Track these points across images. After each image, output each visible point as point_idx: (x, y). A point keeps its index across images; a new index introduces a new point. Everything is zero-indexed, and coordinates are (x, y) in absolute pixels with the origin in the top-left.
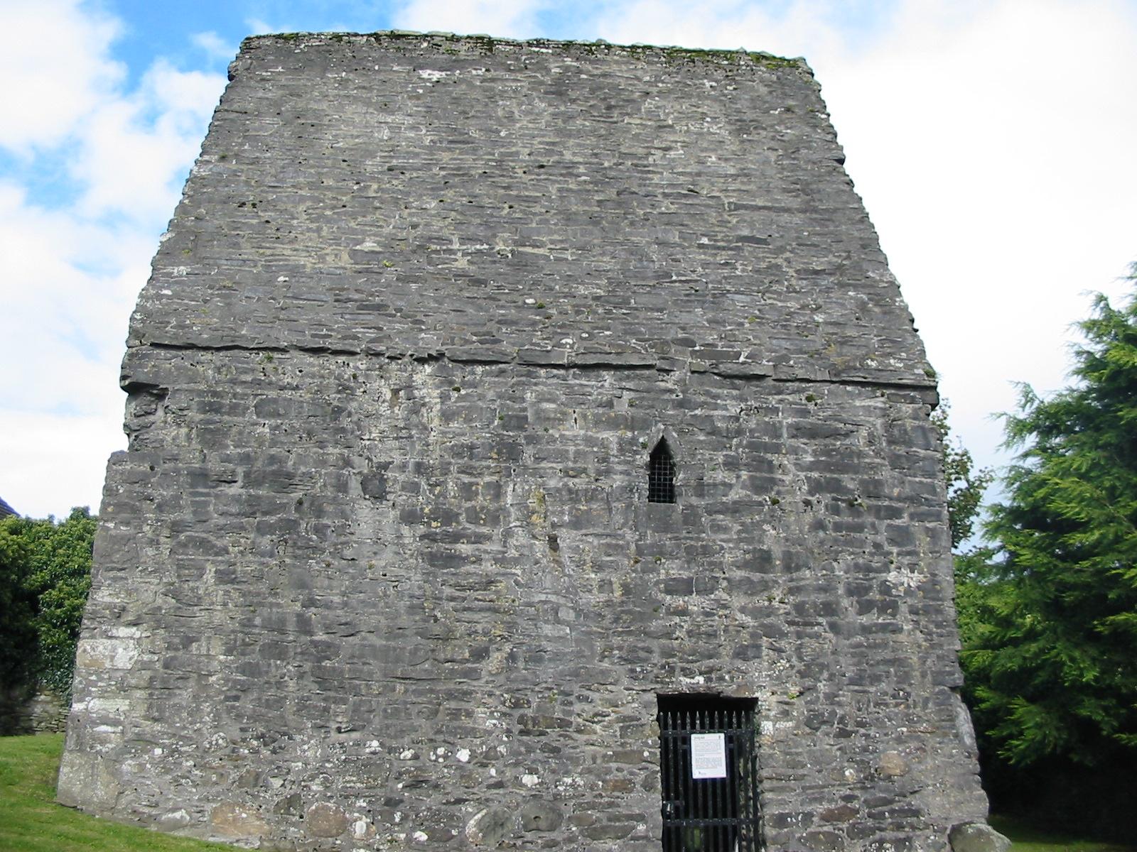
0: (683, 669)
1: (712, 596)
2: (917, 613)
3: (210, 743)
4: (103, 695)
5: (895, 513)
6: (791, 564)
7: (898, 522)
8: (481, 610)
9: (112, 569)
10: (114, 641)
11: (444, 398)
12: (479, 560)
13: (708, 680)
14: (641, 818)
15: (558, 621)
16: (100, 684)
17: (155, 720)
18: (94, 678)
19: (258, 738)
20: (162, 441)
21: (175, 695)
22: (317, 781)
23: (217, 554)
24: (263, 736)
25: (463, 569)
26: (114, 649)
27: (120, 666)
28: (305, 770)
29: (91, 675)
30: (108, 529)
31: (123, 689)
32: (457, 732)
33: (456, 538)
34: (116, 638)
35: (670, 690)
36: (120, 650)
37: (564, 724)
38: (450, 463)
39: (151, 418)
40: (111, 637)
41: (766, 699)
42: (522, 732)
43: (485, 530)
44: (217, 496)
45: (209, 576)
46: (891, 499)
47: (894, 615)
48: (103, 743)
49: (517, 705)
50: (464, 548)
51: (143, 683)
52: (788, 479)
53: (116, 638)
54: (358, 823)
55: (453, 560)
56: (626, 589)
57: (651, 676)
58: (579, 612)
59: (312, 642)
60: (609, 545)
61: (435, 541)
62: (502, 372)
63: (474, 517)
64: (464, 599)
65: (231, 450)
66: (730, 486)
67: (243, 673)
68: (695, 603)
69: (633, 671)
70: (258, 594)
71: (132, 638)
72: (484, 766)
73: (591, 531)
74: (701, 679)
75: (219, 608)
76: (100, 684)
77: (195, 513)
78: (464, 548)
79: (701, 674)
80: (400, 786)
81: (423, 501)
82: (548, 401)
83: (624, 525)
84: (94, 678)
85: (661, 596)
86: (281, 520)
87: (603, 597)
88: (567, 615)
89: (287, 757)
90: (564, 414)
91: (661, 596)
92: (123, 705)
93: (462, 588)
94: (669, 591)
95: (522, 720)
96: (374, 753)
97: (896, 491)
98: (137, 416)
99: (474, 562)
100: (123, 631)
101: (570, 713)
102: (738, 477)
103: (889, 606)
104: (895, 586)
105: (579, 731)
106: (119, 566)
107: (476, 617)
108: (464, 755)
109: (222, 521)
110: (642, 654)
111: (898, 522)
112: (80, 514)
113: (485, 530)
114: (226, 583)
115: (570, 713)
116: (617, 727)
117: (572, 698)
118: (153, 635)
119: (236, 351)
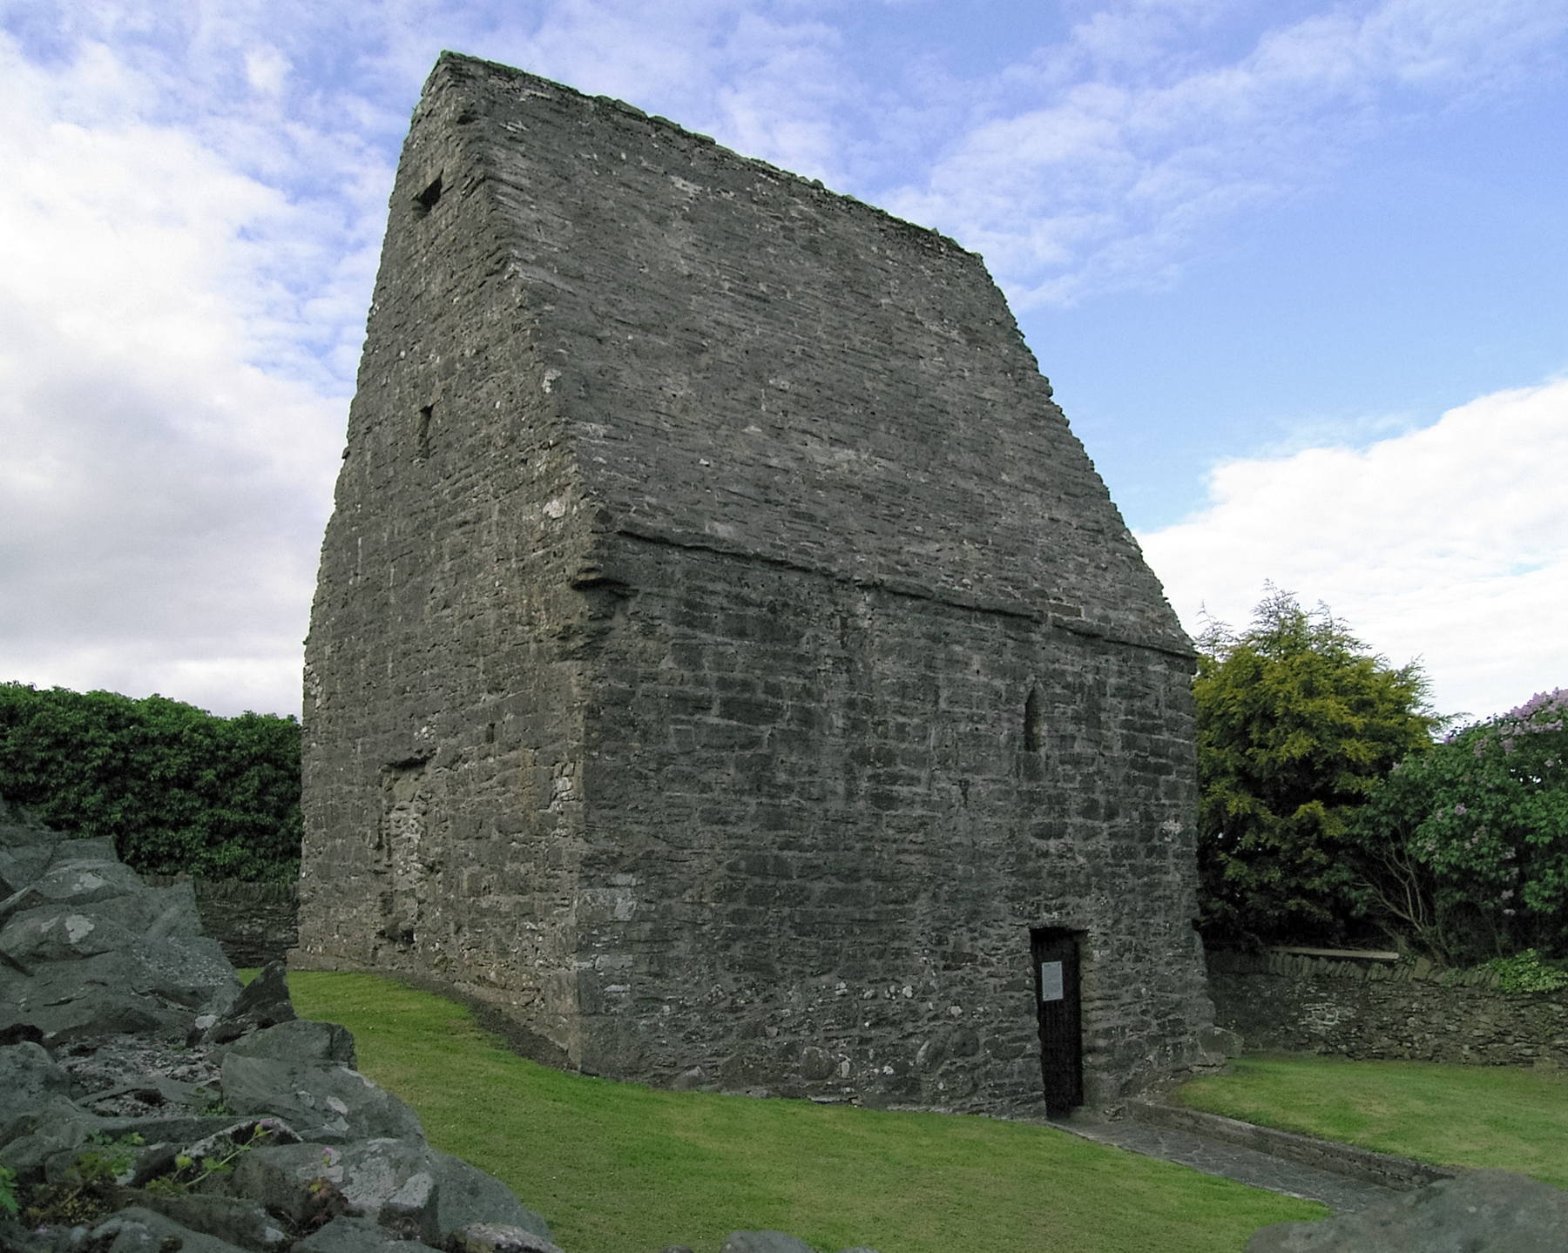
3: (711, 995)
4: (608, 949)
6: (1111, 814)
8: (916, 852)
14: (1028, 1038)
16: (603, 939)
17: (656, 975)
18: (595, 932)
19: (750, 988)
21: (673, 947)
22: (806, 1026)
24: (753, 985)
26: (613, 900)
27: (621, 917)
28: (794, 1015)
29: (593, 929)
31: (627, 944)
32: (893, 975)
33: (894, 779)
34: (614, 886)
35: (1037, 925)
36: (619, 900)
37: (973, 959)
39: (608, 623)
40: (609, 886)
41: (1094, 931)
42: (946, 968)
46: (1167, 757)
48: (616, 1002)
49: (940, 943)
50: (903, 790)
51: (643, 937)
53: (614, 886)
54: (843, 1063)
57: (1026, 913)
62: (924, 608)
67: (733, 921)
68: (1052, 845)
70: (742, 837)
71: (630, 886)
72: (923, 1000)
74: (1055, 914)
75: (707, 851)
76: (603, 939)
77: (679, 744)
78: (903, 790)
80: (867, 1024)
84: (595, 932)
89: (777, 1004)
92: (627, 959)
95: (944, 956)
96: (844, 995)
98: (591, 619)
100: (621, 879)
105: (983, 965)
106: (611, 803)
107: (912, 859)
108: (907, 991)
109: (705, 755)
112: (292, 718)
116: (1006, 960)
118: (648, 882)
119: (705, 553)
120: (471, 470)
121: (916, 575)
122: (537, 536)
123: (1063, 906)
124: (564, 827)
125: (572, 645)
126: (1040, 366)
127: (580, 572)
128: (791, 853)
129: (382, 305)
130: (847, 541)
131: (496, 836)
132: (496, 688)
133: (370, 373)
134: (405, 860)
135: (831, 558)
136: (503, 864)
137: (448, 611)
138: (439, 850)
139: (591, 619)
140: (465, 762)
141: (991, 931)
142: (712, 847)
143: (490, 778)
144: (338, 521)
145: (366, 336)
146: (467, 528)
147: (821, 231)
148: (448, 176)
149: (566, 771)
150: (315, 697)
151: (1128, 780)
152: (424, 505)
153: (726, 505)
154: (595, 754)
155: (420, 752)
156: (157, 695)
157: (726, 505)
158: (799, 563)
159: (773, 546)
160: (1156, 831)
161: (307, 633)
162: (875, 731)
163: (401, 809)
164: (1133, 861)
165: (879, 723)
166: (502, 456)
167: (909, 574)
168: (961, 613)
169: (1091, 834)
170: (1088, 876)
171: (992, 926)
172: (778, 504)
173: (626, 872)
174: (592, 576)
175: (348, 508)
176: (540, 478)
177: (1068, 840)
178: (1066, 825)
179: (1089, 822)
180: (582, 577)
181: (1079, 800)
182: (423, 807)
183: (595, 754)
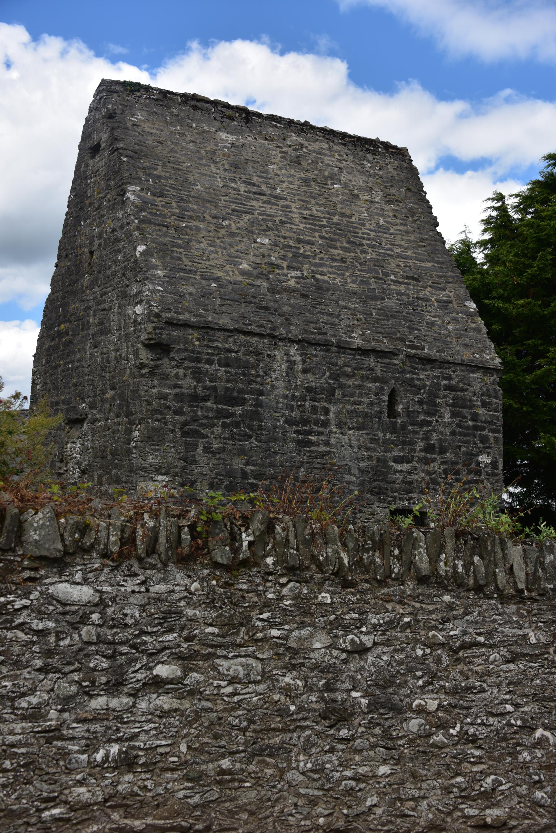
0: (400, 498)
1: (427, 467)
2: (489, 475)
5: (484, 429)
6: (443, 451)
7: (484, 433)
9: (153, 445)
10: (155, 483)
11: (304, 361)
12: (319, 445)
13: (409, 503)
15: (351, 474)
20: (168, 375)
23: (203, 438)
25: (312, 448)
30: (149, 423)
33: (309, 433)
38: (306, 396)
39: (161, 362)
40: (154, 481)
43: (321, 429)
44: (202, 408)
45: (200, 450)
47: (480, 476)
52: (442, 410)
55: (309, 443)
56: (378, 460)
58: (360, 470)
59: (248, 483)
60: (372, 439)
61: (300, 434)
63: (317, 422)
64: (313, 463)
65: (208, 384)
66: (419, 413)
68: (404, 467)
69: (380, 498)
73: (364, 432)
79: (407, 500)
81: (296, 414)
82: (348, 366)
83: (378, 429)
85: (392, 464)
86: (232, 421)
87: (369, 463)
88: (355, 471)
90: (354, 373)
91: (392, 464)
93: (312, 458)
94: (395, 461)
97: (484, 419)
99: (317, 445)
101: (356, 518)
102: (423, 408)
103: (478, 472)
104: (482, 463)
110: (384, 491)
111: (484, 433)
113: (321, 429)
114: (208, 453)
115: (356, 518)
117: (357, 511)
120: (108, 285)
121: (325, 334)
122: (132, 321)
123: (411, 498)
124: (135, 453)
125: (143, 371)
126: (433, 211)
127: (146, 340)
128: (250, 468)
129: (75, 196)
130: (287, 319)
131: (109, 457)
132: (113, 388)
133: (68, 228)
134: (73, 467)
135: (274, 328)
136: (111, 471)
137: (96, 350)
138: (86, 463)
139: (152, 360)
140: (99, 421)
141: (365, 509)
142: (208, 464)
143: (109, 429)
144: (51, 298)
145: (67, 210)
146: (105, 312)
147: (305, 150)
148: (104, 142)
149: (137, 428)
150: (37, 384)
151: (453, 433)
152: (88, 298)
153: (222, 305)
154: (150, 421)
155: (81, 415)
156: (103, 80)
157: (222, 305)
158: (258, 332)
159: (244, 324)
160: (474, 461)
161: (35, 351)
162: (298, 409)
163: (73, 442)
164: (458, 477)
165: (301, 406)
166: (120, 281)
167: (320, 334)
168: (350, 352)
169: (428, 462)
170: (428, 484)
171: (366, 507)
172: (251, 303)
173: (163, 474)
174: (152, 342)
175: (56, 292)
176: (133, 295)
177: (414, 463)
178: (413, 456)
179: (429, 456)
180: (146, 342)
181: (422, 444)
182: (82, 442)
183: (150, 421)
